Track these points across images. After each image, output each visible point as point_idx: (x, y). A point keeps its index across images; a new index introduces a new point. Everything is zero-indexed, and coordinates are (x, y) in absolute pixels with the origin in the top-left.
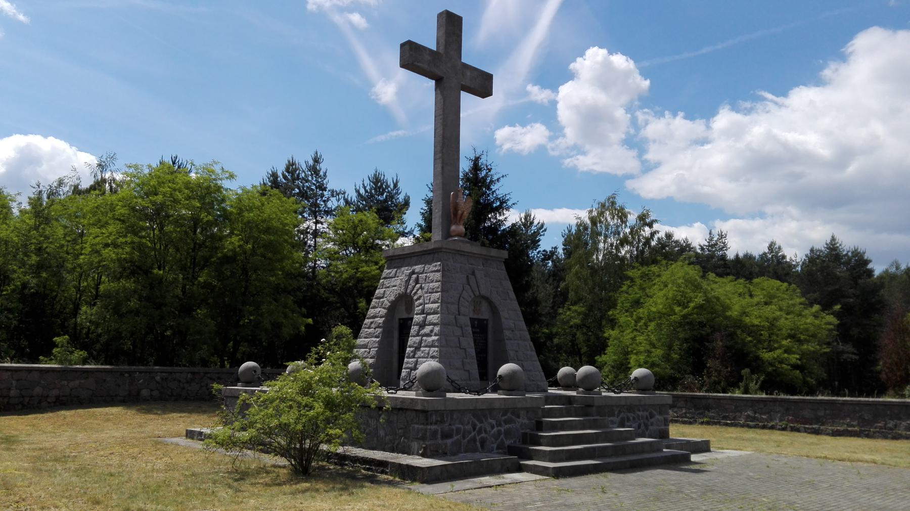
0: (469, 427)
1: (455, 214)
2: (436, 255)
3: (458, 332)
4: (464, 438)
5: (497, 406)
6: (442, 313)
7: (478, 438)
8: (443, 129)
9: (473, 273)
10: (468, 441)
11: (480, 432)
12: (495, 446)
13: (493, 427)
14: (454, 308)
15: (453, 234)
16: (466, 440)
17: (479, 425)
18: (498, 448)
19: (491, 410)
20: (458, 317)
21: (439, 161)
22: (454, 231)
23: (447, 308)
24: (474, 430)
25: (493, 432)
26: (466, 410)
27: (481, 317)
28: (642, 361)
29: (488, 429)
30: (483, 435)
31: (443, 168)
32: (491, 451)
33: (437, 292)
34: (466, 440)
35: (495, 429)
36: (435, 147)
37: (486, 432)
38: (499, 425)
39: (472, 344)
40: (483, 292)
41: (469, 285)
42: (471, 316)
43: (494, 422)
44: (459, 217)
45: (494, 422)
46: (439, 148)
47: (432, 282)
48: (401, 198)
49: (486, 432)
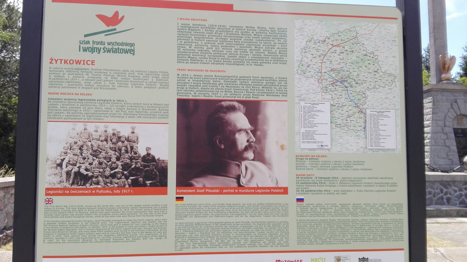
0: (438, 191)
1: (444, 68)
2: (430, 93)
3: (444, 137)
4: (434, 196)
5: (458, 179)
6: (432, 127)
7: (445, 197)
8: (434, 19)
9: (456, 102)
10: (438, 199)
11: (446, 193)
12: (458, 202)
13: (456, 191)
14: (441, 123)
15: (443, 79)
16: (436, 198)
17: (445, 190)
18: (460, 203)
19: (454, 182)
20: (444, 128)
21: (432, 38)
22: (444, 78)
23: (436, 123)
24: (442, 192)
25: (456, 194)
26: (436, 181)
27: (463, 127)
28: (251, 140)
29: (452, 192)
30: (449, 196)
31: (435, 41)
32: (455, 205)
33: (430, 114)
34: (436, 198)
35: (458, 193)
36: (429, 30)
37: (450, 194)
38: (461, 190)
39: (455, 144)
40: (463, 112)
41: (453, 108)
42: (456, 127)
43: (457, 189)
44: (446, 69)
45: (457, 189)
46: (432, 30)
47: (427, 109)
48: (120, 17)
49: (450, 194)
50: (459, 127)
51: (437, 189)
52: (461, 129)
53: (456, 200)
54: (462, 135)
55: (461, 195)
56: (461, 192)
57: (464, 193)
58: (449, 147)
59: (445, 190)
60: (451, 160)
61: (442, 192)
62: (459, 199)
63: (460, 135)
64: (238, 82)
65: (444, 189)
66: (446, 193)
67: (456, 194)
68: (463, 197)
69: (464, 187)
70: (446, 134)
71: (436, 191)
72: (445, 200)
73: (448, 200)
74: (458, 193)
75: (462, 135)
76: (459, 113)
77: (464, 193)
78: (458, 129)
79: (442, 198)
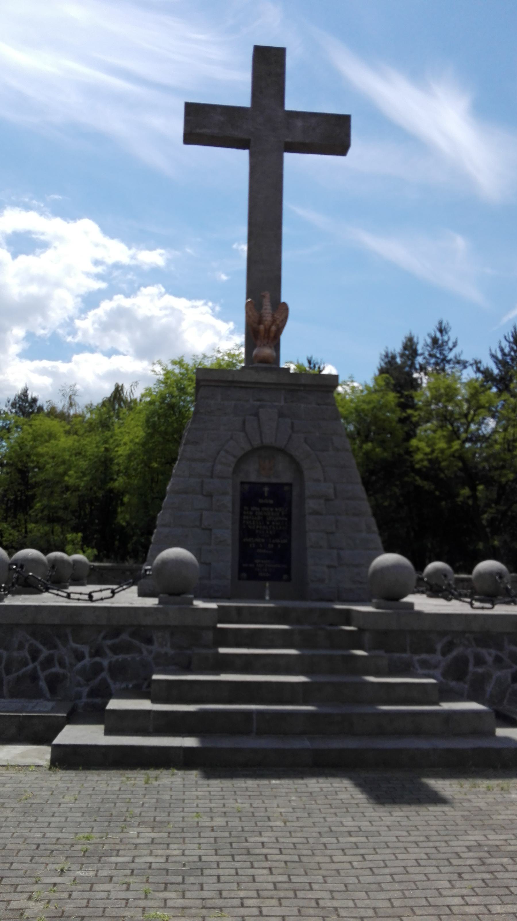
0: (26, 653)
7: (42, 675)
11: (48, 662)
13: (80, 657)
24: (34, 659)
26: (18, 625)
27: (274, 480)
30: (56, 669)
35: (87, 661)
37: (62, 664)
43: (85, 649)
49: (62, 664)
50: (264, 480)
51: (21, 647)
52: (271, 485)
53: (79, 685)
54: (271, 502)
55: (97, 669)
56: (97, 659)
57: (105, 663)
58: (210, 530)
59: (45, 652)
60: (209, 564)
61: (34, 659)
62: (88, 680)
63: (266, 501)
64: (438, 368)
65: (41, 647)
66: (48, 662)
67: (80, 665)
68: (105, 674)
69: (109, 642)
70: (210, 495)
71: (15, 654)
72: (43, 684)
73: (54, 683)
74: (87, 661)
75: (271, 502)
76: (257, 443)
77: (105, 663)
78: (263, 484)
79: (34, 677)
